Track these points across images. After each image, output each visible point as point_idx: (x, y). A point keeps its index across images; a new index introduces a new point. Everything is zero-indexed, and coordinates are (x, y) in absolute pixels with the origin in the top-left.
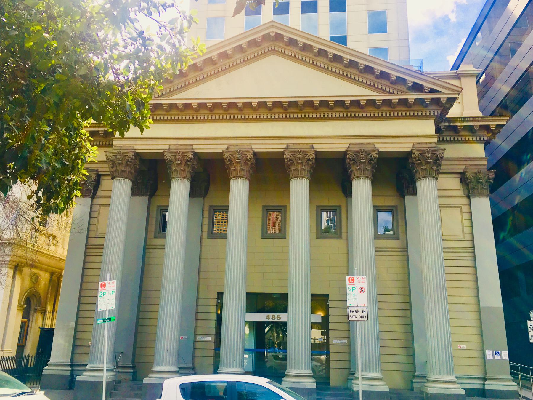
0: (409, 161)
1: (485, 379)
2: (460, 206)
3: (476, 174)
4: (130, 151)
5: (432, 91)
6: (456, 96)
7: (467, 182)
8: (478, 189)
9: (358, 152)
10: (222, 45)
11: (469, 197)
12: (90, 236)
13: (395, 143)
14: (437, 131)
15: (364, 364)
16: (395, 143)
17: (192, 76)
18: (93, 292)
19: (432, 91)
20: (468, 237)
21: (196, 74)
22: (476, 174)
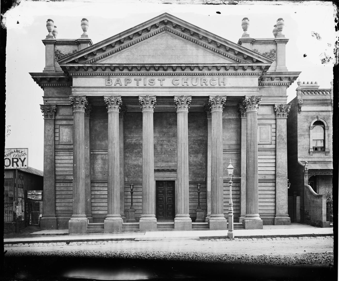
0: (243, 102)
1: (275, 216)
2: (271, 125)
3: (281, 106)
4: (54, 104)
5: (258, 61)
6: (269, 65)
7: (275, 110)
8: (281, 115)
9: (112, 97)
10: (220, 38)
11: (276, 119)
12: (274, 164)
13: (135, 91)
14: (259, 85)
15: (77, 203)
16: (135, 91)
17: (90, 59)
18: (234, 197)
19: (258, 61)
20: (274, 142)
21: (92, 58)
22: (281, 106)
